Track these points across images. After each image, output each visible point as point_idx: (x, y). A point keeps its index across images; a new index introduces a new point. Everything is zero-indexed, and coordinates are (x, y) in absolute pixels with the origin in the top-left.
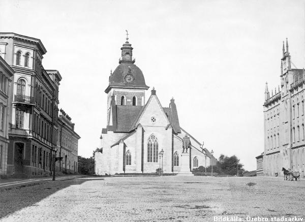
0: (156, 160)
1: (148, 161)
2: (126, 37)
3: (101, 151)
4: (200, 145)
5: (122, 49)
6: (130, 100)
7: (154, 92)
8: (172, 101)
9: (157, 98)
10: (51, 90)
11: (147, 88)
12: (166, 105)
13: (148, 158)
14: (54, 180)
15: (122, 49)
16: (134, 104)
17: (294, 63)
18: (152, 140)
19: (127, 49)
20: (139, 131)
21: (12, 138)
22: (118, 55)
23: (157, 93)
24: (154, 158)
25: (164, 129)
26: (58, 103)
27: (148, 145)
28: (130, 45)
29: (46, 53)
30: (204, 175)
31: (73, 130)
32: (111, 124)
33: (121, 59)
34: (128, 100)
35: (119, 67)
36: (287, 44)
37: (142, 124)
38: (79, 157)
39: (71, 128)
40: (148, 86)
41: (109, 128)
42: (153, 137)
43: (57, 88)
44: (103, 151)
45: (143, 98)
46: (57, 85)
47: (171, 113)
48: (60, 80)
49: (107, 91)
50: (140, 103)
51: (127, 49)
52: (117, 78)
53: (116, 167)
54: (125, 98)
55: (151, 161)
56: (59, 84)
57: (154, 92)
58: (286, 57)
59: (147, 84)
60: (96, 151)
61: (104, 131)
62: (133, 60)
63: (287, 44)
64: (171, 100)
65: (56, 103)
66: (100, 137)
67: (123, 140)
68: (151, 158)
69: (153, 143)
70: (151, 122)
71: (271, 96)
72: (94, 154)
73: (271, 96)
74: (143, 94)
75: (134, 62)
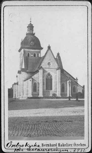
1: (46, 89)
2: (30, 21)
3: (17, 84)
6: (32, 55)
8: (58, 54)
9: (51, 51)
12: (56, 56)
15: (28, 27)
19: (31, 27)
21: (30, 30)
22: (25, 31)
27: (46, 79)
28: (32, 25)
30: (71, 107)
32: (23, 67)
33: (27, 33)
34: (31, 55)
35: (26, 37)
37: (43, 67)
40: (43, 47)
41: (23, 70)
44: (19, 83)
45: (40, 54)
47: (58, 59)
51: (31, 27)
52: (24, 43)
53: (27, 93)
54: (30, 54)
59: (42, 46)
60: (14, 84)
61: (19, 72)
62: (34, 33)
64: (57, 54)
66: (16, 76)
69: (49, 78)
70: (48, 66)
72: (13, 86)
74: (40, 52)
75: (34, 34)
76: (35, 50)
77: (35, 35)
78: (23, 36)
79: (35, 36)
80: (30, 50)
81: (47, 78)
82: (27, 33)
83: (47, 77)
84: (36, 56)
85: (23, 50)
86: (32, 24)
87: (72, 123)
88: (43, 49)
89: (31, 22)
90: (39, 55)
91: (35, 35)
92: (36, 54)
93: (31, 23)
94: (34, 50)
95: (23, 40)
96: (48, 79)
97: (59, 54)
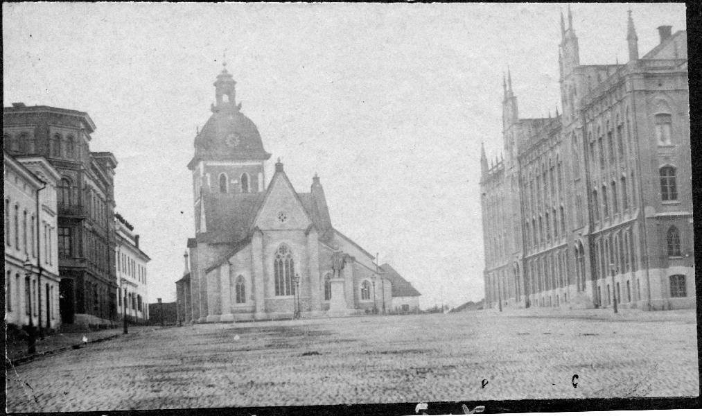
0: (673, 278)
1: (277, 293)
4: (373, 258)
5: (215, 85)
6: (236, 182)
7: (279, 167)
10: (103, 187)
11: (267, 156)
13: (277, 288)
14: (126, 332)
16: (245, 187)
17: (343, 232)
18: (281, 254)
19: (225, 85)
20: (257, 241)
23: (285, 168)
24: (288, 288)
25: (302, 234)
26: (114, 206)
29: (95, 131)
31: (137, 246)
32: (204, 228)
35: (211, 121)
36: (509, 77)
37: (261, 227)
38: (493, 297)
39: (134, 243)
42: (283, 249)
43: (112, 180)
45: (260, 175)
46: (112, 175)
48: (115, 167)
49: (192, 166)
50: (255, 185)
51: (225, 85)
52: (205, 142)
54: (227, 178)
55: (283, 294)
56: (114, 174)
57: (279, 167)
58: (510, 100)
59: (267, 149)
63: (509, 77)
64: (314, 178)
65: (111, 207)
67: (228, 259)
68: (282, 287)
69: (284, 260)
71: (490, 167)
73: (490, 167)
74: (261, 169)
76: (242, 164)
77: (241, 111)
78: (202, 116)
79: (242, 114)
80: (222, 164)
81: (278, 260)
82: (212, 105)
83: (278, 257)
84: (227, 189)
85: (201, 165)
86: (230, 72)
87: (327, 156)
88: (661, 24)
89: (227, 68)
90: (257, 178)
91: (241, 111)
92: (247, 173)
93: (225, 71)
94: (238, 164)
95: (200, 131)
96: (281, 262)
97: (319, 178)
